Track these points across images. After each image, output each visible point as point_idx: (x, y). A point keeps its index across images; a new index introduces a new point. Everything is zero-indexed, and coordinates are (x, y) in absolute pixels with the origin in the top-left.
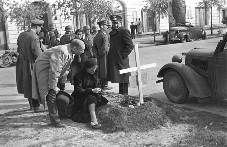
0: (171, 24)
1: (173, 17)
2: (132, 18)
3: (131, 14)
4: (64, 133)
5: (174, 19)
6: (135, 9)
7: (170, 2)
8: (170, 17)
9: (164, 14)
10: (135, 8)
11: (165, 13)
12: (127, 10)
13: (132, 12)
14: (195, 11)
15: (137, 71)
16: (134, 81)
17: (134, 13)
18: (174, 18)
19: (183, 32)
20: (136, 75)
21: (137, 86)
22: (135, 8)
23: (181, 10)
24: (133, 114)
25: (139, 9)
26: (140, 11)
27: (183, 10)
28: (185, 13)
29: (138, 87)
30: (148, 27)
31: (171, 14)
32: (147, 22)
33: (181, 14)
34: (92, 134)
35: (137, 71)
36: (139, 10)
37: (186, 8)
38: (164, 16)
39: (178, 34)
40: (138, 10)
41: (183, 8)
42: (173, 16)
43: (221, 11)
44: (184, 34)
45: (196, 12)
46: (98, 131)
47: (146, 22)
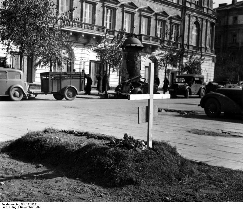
0: (124, 77)
1: (127, 70)
2: (79, 68)
3: (79, 63)
4: (181, 148)
5: (127, 72)
6: (83, 58)
7: (125, 55)
8: (124, 70)
9: (115, 67)
10: (84, 58)
11: (116, 66)
12: (75, 58)
13: (80, 62)
14: (144, 70)
15: (149, 100)
16: (144, 114)
17: (82, 62)
18: (128, 72)
19: (137, 88)
20: (147, 105)
21: (146, 122)
22: (84, 58)
23: (136, 64)
24: (143, 160)
25: (87, 59)
26: (89, 61)
27: (138, 64)
28: (139, 68)
29: (147, 123)
30: (95, 80)
31: (125, 67)
32: (95, 75)
33: (135, 69)
34: (32, 188)
35: (149, 100)
36: (88, 60)
37: (141, 63)
38: (115, 69)
39: (132, 89)
40: (86, 60)
41: (139, 62)
42: (127, 70)
43: (170, 74)
44: (139, 90)
45: (145, 71)
46: (77, 180)
47: (93, 74)
